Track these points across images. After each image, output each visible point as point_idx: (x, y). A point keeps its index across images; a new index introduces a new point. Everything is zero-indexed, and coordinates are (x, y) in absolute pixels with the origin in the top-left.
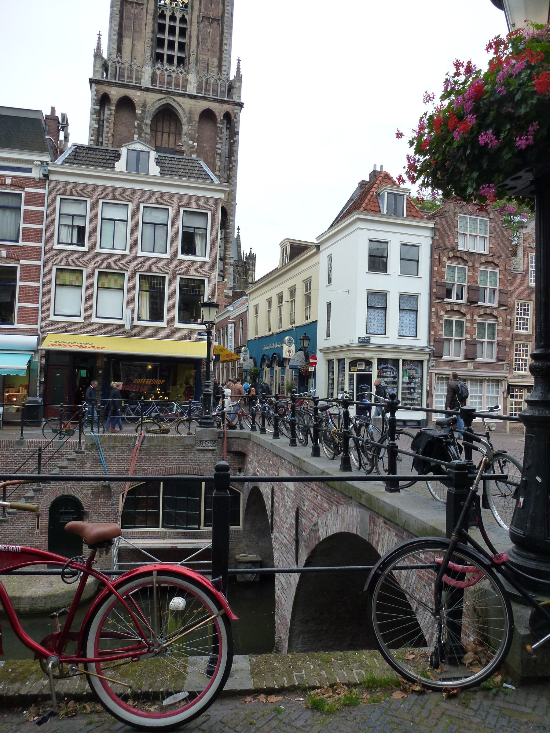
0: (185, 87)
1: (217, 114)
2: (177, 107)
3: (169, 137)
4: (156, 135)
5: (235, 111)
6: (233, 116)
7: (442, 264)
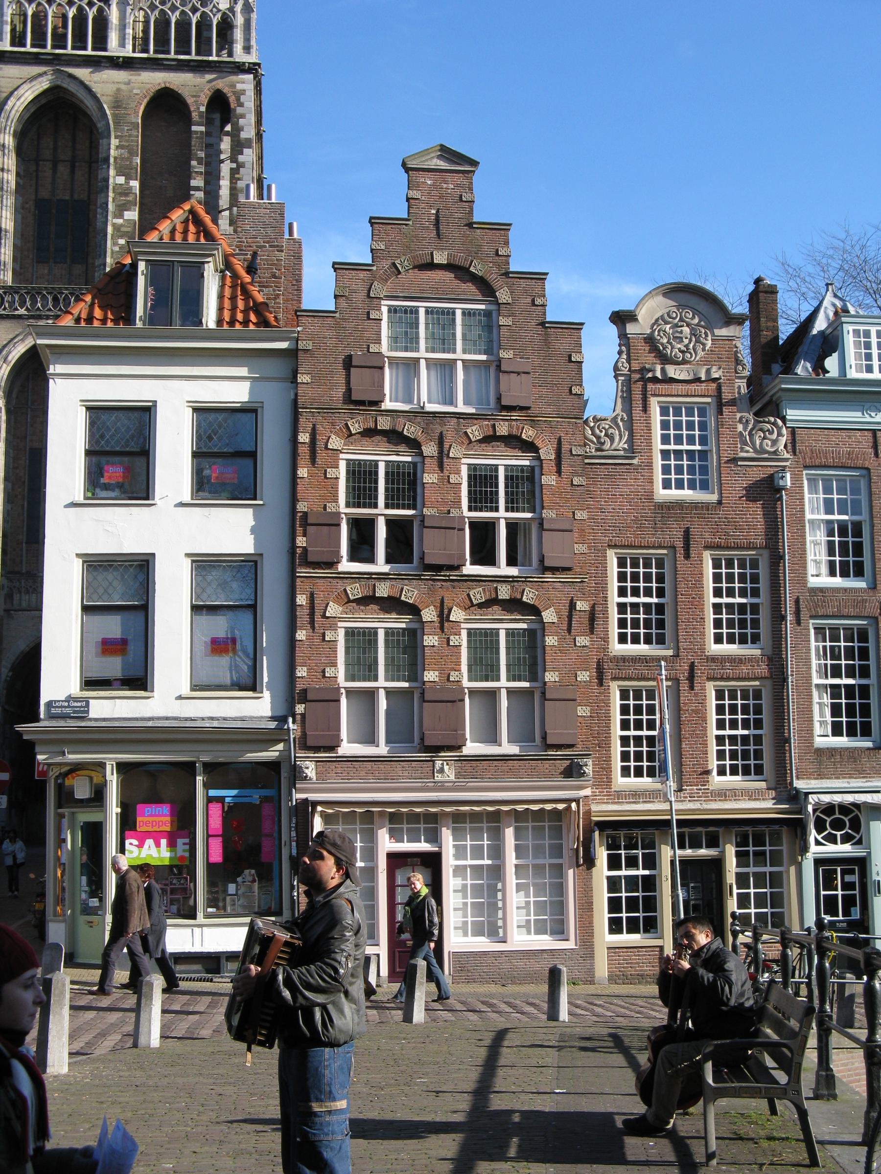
0: (101, 41)
1: (190, 101)
2: (81, 94)
3: (73, 171)
4: (37, 171)
5: (239, 87)
6: (232, 100)
7: (321, 456)
